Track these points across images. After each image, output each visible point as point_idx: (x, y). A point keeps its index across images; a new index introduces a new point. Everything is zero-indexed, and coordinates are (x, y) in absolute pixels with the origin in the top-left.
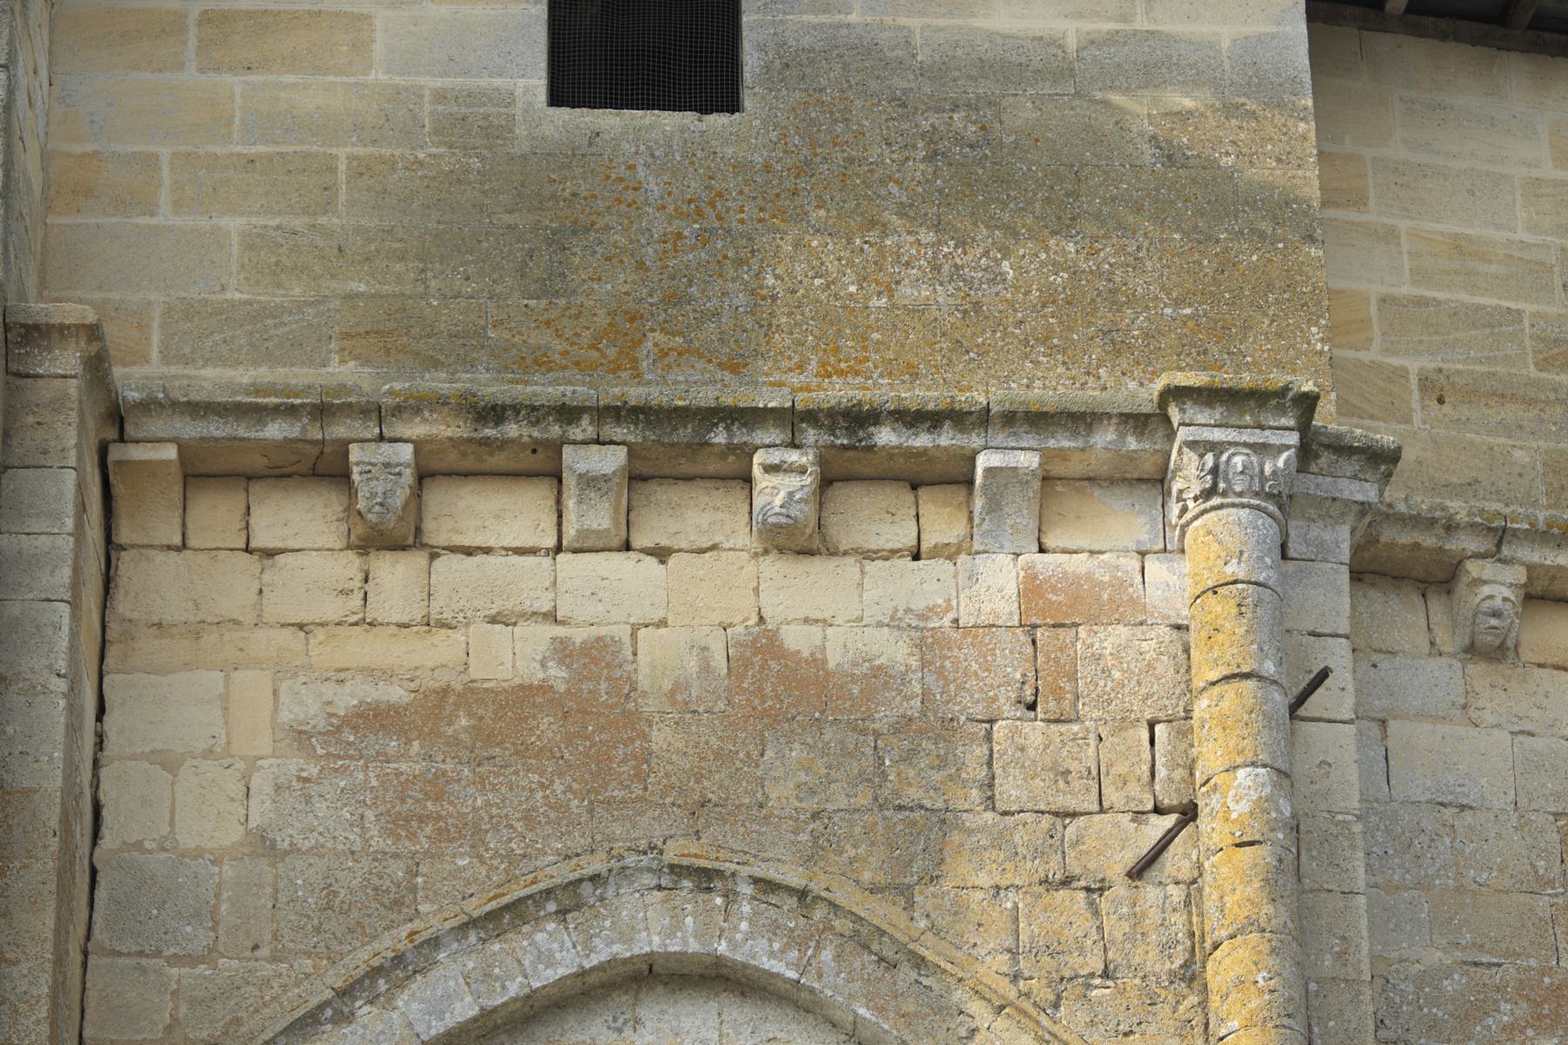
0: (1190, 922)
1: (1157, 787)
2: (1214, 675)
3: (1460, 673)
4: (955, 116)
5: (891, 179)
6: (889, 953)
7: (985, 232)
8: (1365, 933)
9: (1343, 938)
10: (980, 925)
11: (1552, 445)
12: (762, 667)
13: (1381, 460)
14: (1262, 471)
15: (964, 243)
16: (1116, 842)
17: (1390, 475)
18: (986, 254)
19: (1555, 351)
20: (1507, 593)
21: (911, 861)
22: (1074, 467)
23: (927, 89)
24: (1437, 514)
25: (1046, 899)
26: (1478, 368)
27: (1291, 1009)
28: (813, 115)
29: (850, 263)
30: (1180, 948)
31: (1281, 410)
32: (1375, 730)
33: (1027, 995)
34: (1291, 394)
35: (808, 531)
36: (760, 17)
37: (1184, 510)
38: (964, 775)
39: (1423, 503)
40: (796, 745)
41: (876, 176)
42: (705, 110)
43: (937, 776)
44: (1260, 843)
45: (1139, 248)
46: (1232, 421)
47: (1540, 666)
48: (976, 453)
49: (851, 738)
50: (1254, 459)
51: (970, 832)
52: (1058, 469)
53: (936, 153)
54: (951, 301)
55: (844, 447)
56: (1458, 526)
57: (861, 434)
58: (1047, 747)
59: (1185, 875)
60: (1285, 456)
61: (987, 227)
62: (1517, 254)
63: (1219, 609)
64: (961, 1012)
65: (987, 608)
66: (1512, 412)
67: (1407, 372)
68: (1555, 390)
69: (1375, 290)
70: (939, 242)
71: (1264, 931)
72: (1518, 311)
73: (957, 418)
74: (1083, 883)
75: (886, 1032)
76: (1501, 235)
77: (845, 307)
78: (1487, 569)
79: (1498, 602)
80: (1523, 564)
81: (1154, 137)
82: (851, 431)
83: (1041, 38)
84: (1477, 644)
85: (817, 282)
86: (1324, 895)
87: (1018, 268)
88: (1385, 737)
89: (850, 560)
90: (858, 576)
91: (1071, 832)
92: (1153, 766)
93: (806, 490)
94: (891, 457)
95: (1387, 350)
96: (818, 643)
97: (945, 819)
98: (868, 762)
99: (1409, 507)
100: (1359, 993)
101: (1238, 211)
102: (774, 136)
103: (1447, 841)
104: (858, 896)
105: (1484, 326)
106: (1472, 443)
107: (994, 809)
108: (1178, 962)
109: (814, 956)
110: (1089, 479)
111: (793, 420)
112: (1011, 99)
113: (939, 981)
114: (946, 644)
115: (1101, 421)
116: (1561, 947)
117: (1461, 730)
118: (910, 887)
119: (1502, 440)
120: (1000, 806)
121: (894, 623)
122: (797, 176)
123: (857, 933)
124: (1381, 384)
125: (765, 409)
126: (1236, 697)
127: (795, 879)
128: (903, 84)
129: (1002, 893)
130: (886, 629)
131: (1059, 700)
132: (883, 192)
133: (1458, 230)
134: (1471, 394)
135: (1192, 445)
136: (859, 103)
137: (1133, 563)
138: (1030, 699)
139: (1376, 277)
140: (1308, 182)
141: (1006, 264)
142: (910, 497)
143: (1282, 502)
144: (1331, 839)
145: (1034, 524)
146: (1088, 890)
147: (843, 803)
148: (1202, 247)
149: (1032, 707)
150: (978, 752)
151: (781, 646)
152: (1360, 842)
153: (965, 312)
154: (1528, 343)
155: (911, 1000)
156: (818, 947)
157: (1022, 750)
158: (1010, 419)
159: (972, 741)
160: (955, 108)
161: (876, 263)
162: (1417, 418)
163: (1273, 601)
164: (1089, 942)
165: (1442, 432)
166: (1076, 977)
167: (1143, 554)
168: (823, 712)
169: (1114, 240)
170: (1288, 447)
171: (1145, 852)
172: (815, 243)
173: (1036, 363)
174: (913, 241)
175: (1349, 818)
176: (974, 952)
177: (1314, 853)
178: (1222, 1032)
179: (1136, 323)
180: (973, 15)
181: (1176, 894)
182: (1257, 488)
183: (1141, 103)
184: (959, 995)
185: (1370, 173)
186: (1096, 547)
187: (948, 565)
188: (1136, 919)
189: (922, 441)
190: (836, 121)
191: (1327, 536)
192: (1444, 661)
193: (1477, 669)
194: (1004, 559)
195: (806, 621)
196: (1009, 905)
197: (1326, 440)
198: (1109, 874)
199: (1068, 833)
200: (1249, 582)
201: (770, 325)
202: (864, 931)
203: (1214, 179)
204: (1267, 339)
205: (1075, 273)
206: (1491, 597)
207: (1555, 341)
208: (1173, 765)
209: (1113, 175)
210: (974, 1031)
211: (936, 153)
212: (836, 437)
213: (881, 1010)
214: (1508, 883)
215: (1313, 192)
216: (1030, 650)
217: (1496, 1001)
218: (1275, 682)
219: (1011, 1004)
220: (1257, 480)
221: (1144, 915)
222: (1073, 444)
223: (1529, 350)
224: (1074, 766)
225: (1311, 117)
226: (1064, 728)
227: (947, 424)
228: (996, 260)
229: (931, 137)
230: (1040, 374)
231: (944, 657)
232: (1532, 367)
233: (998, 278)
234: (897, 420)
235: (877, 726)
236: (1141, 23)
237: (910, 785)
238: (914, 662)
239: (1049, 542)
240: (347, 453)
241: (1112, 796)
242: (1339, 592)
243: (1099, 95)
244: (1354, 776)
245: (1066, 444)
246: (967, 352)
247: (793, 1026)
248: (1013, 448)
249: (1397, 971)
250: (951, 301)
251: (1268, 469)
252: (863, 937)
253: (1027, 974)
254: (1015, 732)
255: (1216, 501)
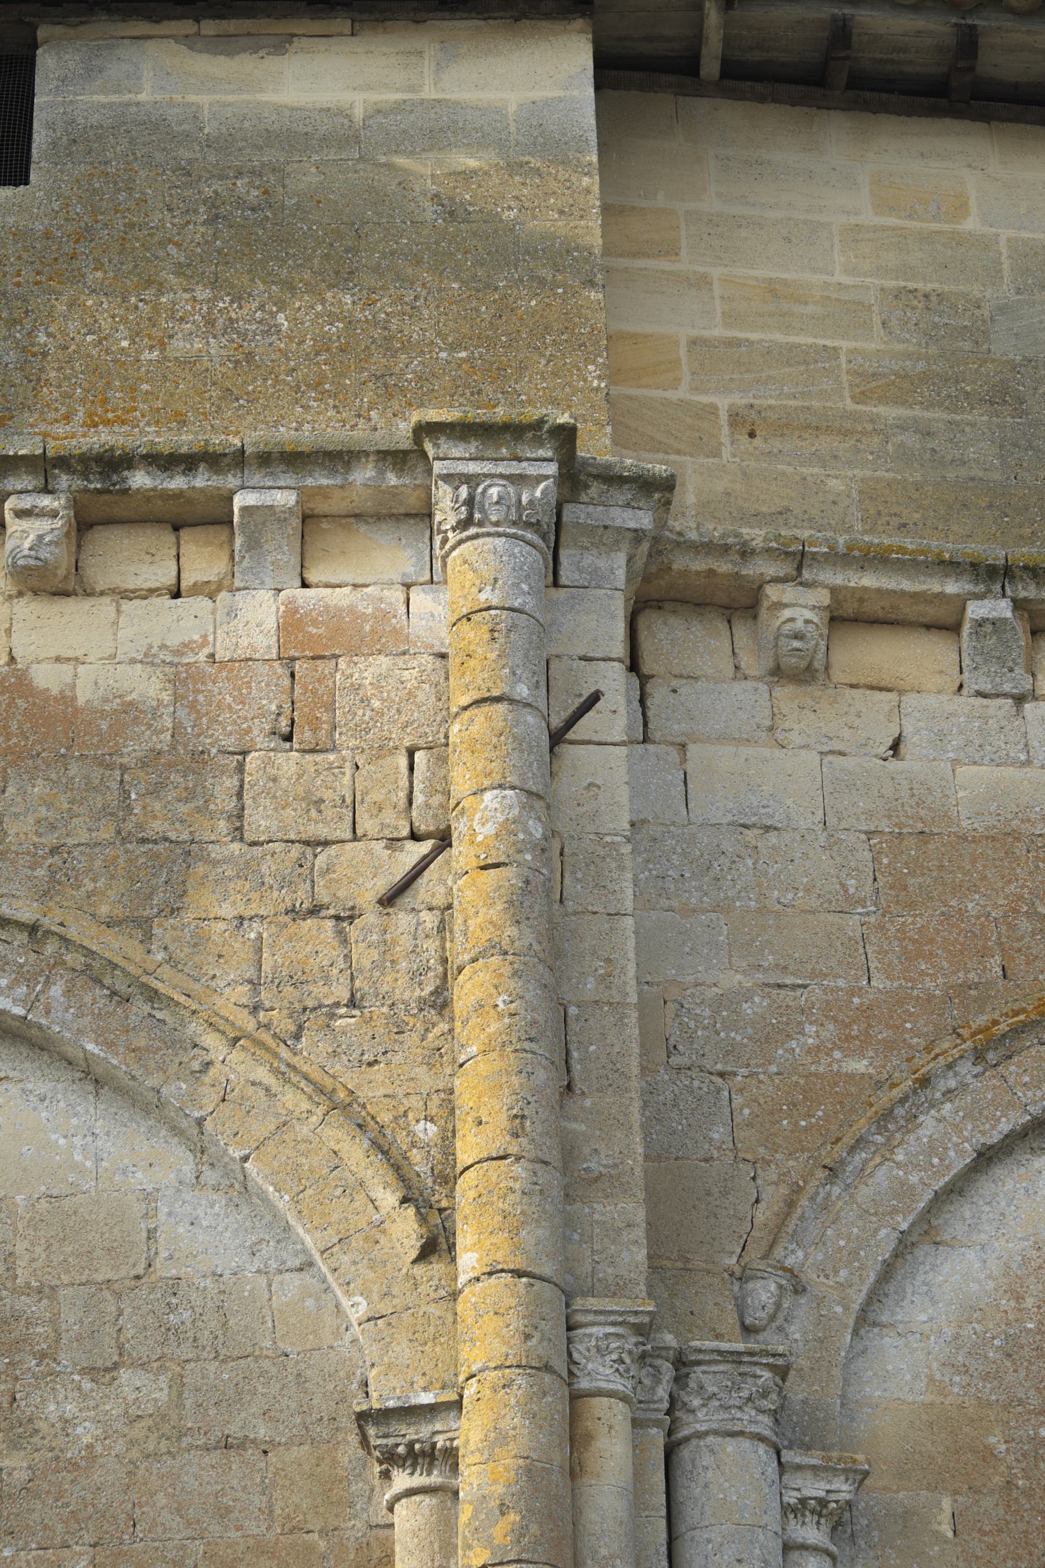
0: (444, 948)
1: (414, 814)
2: (465, 700)
3: (767, 695)
4: (239, 183)
5: (170, 241)
6: (121, 987)
7: (262, 287)
8: (632, 955)
9: (608, 960)
10: (220, 956)
11: (868, 473)
12: (9, 705)
13: (658, 489)
14: (520, 501)
15: (240, 298)
16: (364, 870)
17: (669, 503)
18: (262, 307)
19: (874, 384)
20: (809, 615)
21: (152, 893)
22: (337, 504)
23: (212, 159)
24: (730, 540)
25: (293, 928)
26: (791, 403)
27: (533, 1033)
28: (97, 185)
29: (124, 320)
30: (431, 974)
31: (538, 442)
32: (674, 754)
33: (267, 1027)
34: (547, 426)
35: (61, 573)
36: (51, 98)
37: (445, 541)
38: (212, 807)
39: (714, 530)
40: (39, 781)
41: (156, 239)
42: (16, 185)
43: (183, 809)
44: (505, 864)
45: (416, 298)
46: (489, 453)
47: (852, 686)
48: (233, 493)
49: (97, 773)
50: (511, 489)
51: (215, 863)
52: (321, 507)
53: (217, 217)
54: (223, 352)
55: (98, 491)
56: (753, 552)
57: (115, 477)
58: (300, 776)
59: (439, 901)
60: (542, 486)
61: (264, 282)
62: (834, 296)
63: (472, 635)
64: (196, 1046)
65: (244, 642)
66: (825, 443)
67: (716, 408)
68: (872, 421)
69: (684, 333)
70: (215, 299)
71: (506, 953)
72: (835, 349)
73: (211, 460)
74: (332, 912)
75: (115, 1067)
76: (820, 278)
77: (115, 361)
78: (788, 593)
79: (799, 625)
80: (826, 587)
81: (437, 196)
82: (104, 476)
83: (329, 109)
84: (783, 666)
85: (89, 338)
86: (588, 917)
87: (293, 320)
88: (684, 760)
89: (106, 600)
90: (113, 615)
91: (321, 861)
92: (411, 792)
93: (56, 532)
94: (148, 500)
95: (697, 389)
96: (69, 680)
97: (190, 851)
98: (113, 797)
99: (701, 535)
100: (624, 1016)
101: (518, 260)
102: (56, 206)
103: (750, 862)
104: (94, 930)
105: (799, 363)
106: (783, 474)
107: (242, 839)
108: (429, 989)
109: (43, 991)
110: (356, 516)
111: (46, 467)
112: (295, 166)
113: (174, 1014)
114: (202, 678)
115: (359, 459)
116: (872, 966)
117: (766, 752)
118: (149, 920)
119: (816, 470)
120: (249, 836)
121: (148, 660)
122: (77, 241)
123: (89, 966)
124: (689, 420)
125: (16, 457)
126: (481, 723)
127: (26, 915)
128: (188, 155)
129: (246, 923)
130: (139, 665)
131: (314, 731)
132: (161, 254)
133: (774, 275)
134: (784, 427)
135: (447, 478)
136: (143, 173)
137: (397, 595)
138: (285, 730)
139: (680, 321)
140: (591, 231)
141: (281, 318)
142: (172, 538)
143: (552, 535)
144: (598, 861)
145: (295, 560)
146: (338, 918)
147: (84, 837)
148: (480, 295)
149: (288, 738)
150: (228, 783)
151: (30, 685)
152: (628, 863)
153: (237, 362)
154: (844, 378)
155: (143, 1034)
156: (47, 982)
157: (275, 780)
158: (266, 460)
159: (223, 773)
160: (239, 174)
161: (149, 319)
162: (726, 452)
163: (534, 634)
164: (335, 971)
165: (753, 464)
166: (320, 1006)
167: (408, 586)
168: (68, 748)
169: (392, 292)
170: (546, 477)
171: (399, 878)
172: (90, 303)
173: (306, 408)
174: (188, 299)
175: (619, 839)
176: (213, 984)
177: (579, 875)
178: (462, 1058)
179: (409, 367)
180: (262, 91)
181: (430, 920)
182: (513, 517)
183: (426, 165)
184: (194, 1027)
185: (683, 226)
186: (360, 580)
187: (207, 603)
188: (386, 946)
189: (177, 483)
190: (119, 190)
191: (602, 563)
192: (750, 684)
193: (784, 692)
194: (265, 595)
195: (58, 659)
196: (253, 936)
197: (595, 471)
198: (360, 902)
199: (317, 862)
200: (503, 608)
201: (39, 380)
202: (96, 965)
203: (496, 231)
204: (543, 378)
205: (350, 323)
206: (792, 620)
207: (874, 375)
208: (430, 792)
209: (393, 231)
210: (208, 1064)
211: (217, 217)
212: (89, 481)
213: (110, 1045)
214: (814, 903)
215: (597, 241)
216: (287, 682)
217: (800, 1023)
218: (528, 705)
219: (248, 1036)
220: (513, 510)
221: (395, 942)
222: (331, 482)
223: (846, 385)
224: (328, 795)
225: (596, 172)
226: (319, 758)
227: (202, 467)
228: (271, 313)
229: (213, 203)
230: (309, 418)
231: (197, 691)
232: (848, 401)
233: (271, 330)
234: (150, 464)
235: (125, 760)
236: (429, 93)
237: (155, 817)
238: (166, 697)
239: (311, 577)
240: (964, 609)
241: (367, 824)
242: (613, 617)
243: (383, 159)
244: (623, 795)
245: (325, 482)
246: (237, 399)
247: (27, 1065)
248: (270, 488)
249: (693, 995)
250: (223, 352)
251: (525, 499)
252: (94, 971)
253: (267, 1004)
254: (268, 763)
255: (472, 531)
